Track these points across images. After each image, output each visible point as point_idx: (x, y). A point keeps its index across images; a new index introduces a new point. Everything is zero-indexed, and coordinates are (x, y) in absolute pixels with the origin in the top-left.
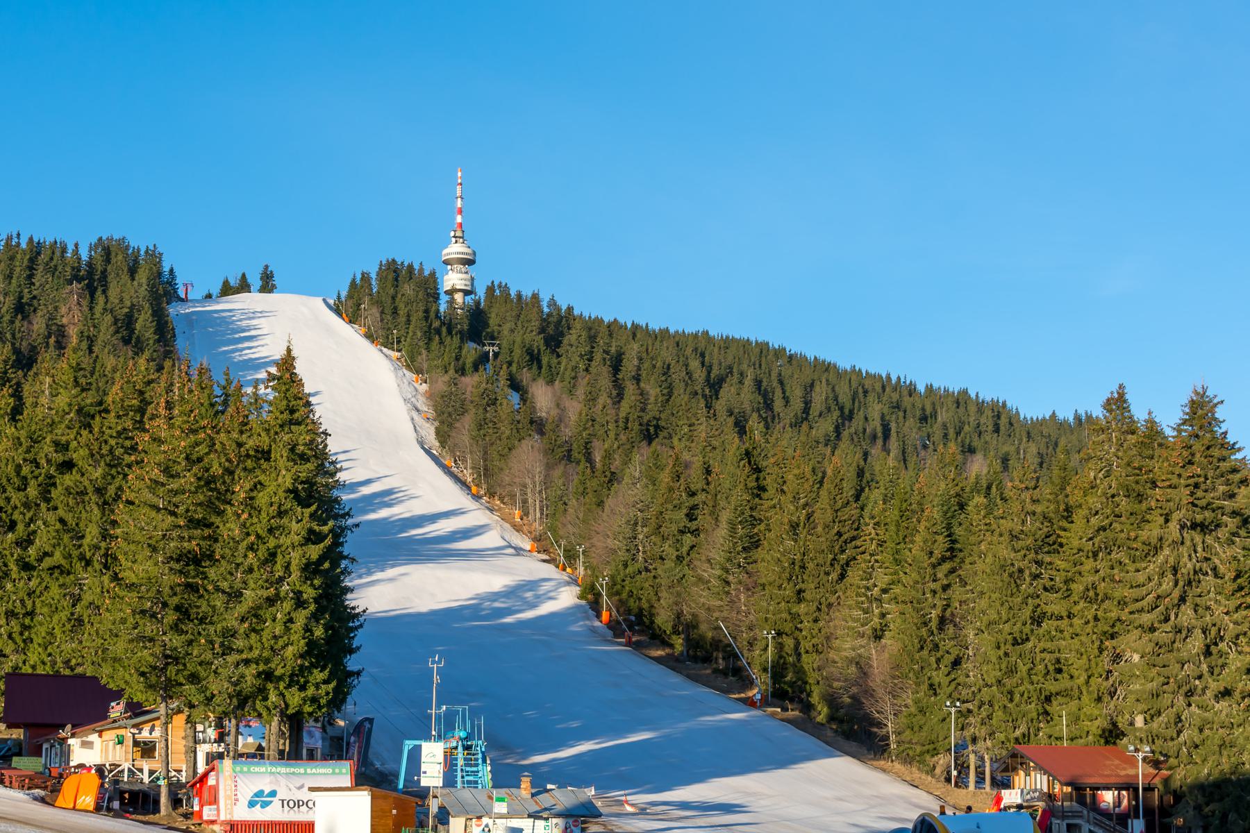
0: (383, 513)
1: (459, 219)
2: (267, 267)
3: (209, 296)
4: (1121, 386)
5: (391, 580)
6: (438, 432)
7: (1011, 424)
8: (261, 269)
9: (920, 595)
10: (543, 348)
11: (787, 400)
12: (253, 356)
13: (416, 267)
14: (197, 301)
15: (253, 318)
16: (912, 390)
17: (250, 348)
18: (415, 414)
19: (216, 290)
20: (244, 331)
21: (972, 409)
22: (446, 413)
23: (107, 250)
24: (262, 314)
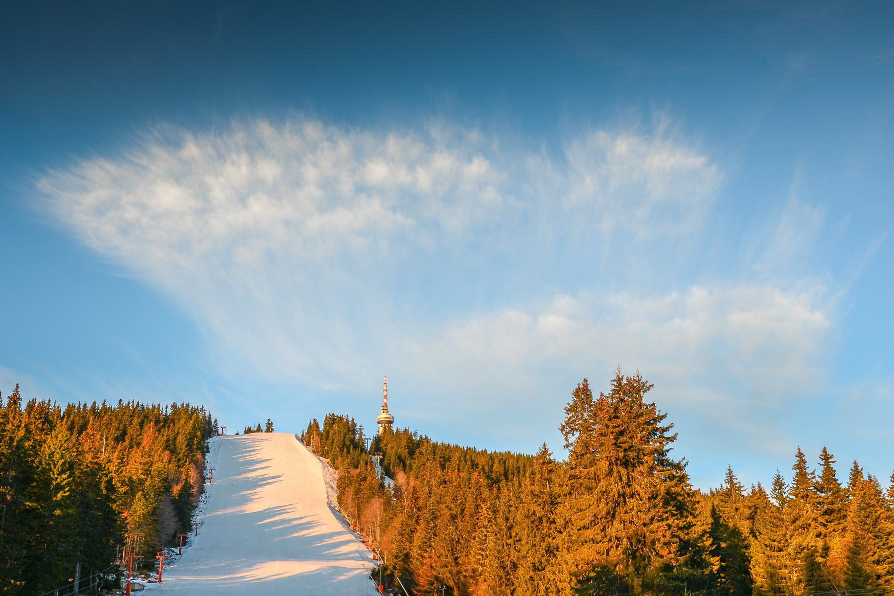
0: (304, 532)
3: (237, 434)
4: (585, 380)
9: (500, 548)
18: (329, 490)
23: (176, 410)
24: (263, 440)
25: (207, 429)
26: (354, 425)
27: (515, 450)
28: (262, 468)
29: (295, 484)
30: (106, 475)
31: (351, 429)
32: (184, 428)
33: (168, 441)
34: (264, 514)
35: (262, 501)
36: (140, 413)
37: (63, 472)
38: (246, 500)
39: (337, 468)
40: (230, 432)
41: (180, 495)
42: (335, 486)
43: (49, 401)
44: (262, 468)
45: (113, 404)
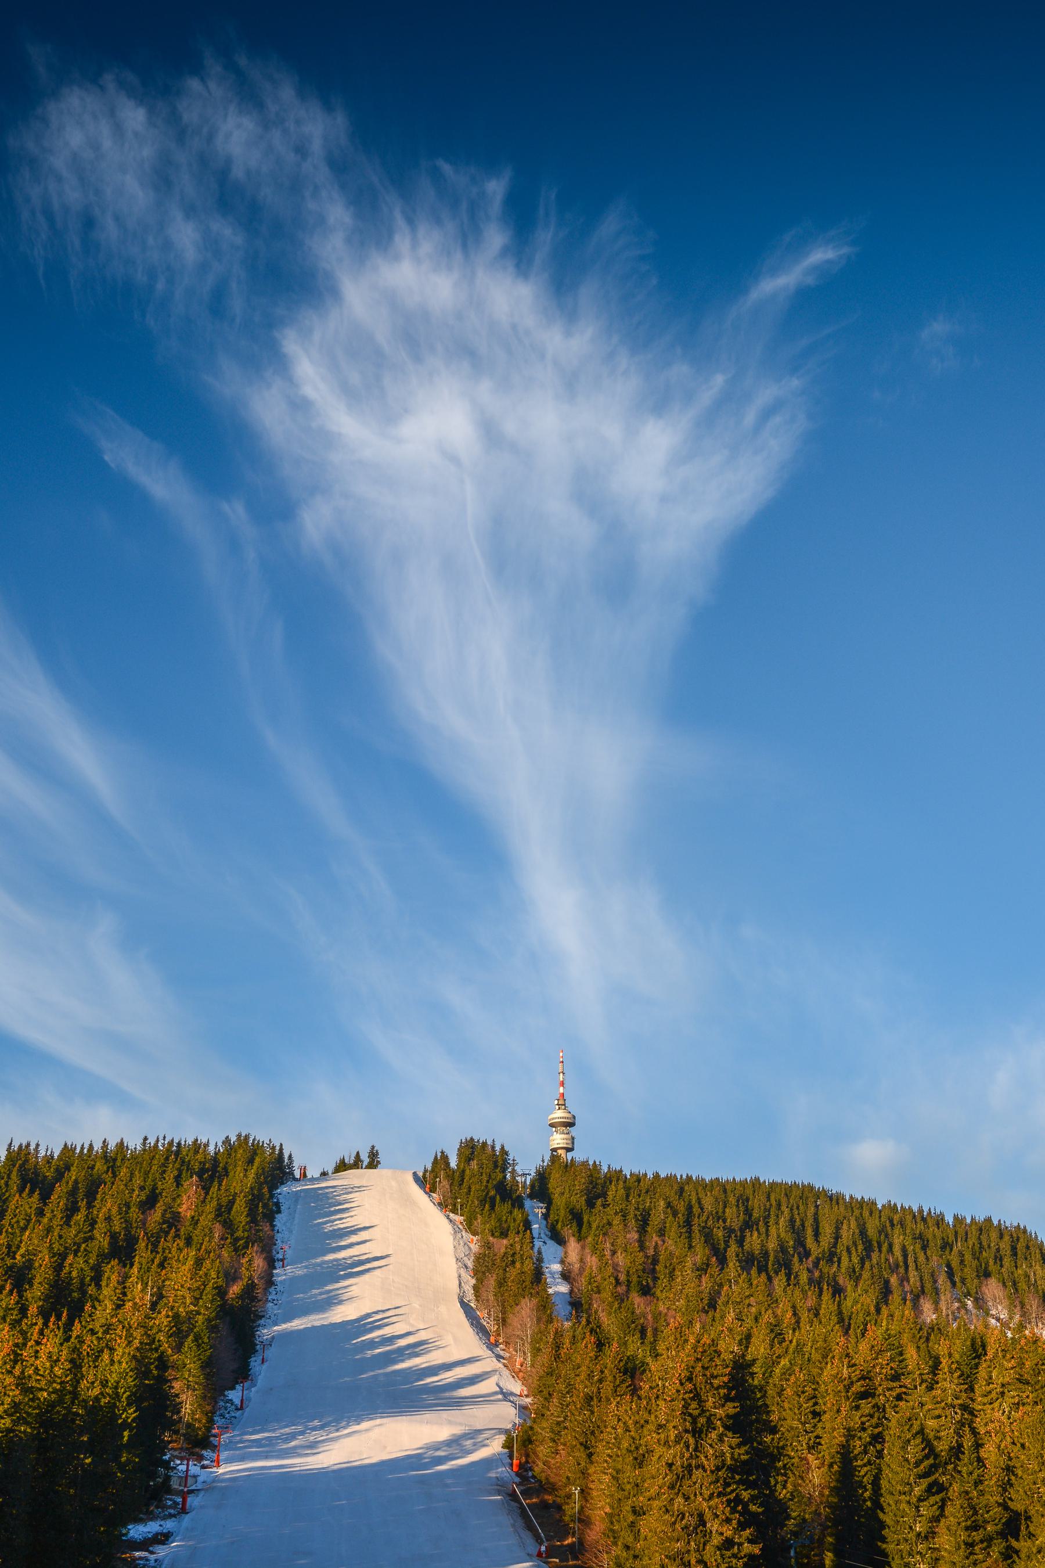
1: (561, 1090)
2: (373, 1147)
3: (324, 1174)
5: (367, 1430)
6: (476, 1288)
7: (1028, 1247)
8: (368, 1150)
10: (584, 1208)
11: (817, 1234)
12: (342, 1226)
13: (489, 1142)
14: (317, 1179)
15: (351, 1193)
16: (939, 1221)
17: (340, 1219)
18: (463, 1271)
19: (330, 1169)
20: (340, 1204)
21: (994, 1235)
22: (483, 1267)
24: (359, 1189)
25: (278, 1170)
26: (504, 1152)
27: (768, 1176)
28: (358, 1243)
29: (404, 1264)
30: (156, 1350)
31: (500, 1161)
32: (241, 1181)
34: (361, 1325)
35: (359, 1299)
36: (178, 1153)
37: (129, 1405)
38: (332, 1301)
39: (474, 1234)
40: (313, 1172)
41: (240, 1297)
42: (470, 1264)
43: (38, 1145)
44: (358, 1243)
45: (134, 1143)
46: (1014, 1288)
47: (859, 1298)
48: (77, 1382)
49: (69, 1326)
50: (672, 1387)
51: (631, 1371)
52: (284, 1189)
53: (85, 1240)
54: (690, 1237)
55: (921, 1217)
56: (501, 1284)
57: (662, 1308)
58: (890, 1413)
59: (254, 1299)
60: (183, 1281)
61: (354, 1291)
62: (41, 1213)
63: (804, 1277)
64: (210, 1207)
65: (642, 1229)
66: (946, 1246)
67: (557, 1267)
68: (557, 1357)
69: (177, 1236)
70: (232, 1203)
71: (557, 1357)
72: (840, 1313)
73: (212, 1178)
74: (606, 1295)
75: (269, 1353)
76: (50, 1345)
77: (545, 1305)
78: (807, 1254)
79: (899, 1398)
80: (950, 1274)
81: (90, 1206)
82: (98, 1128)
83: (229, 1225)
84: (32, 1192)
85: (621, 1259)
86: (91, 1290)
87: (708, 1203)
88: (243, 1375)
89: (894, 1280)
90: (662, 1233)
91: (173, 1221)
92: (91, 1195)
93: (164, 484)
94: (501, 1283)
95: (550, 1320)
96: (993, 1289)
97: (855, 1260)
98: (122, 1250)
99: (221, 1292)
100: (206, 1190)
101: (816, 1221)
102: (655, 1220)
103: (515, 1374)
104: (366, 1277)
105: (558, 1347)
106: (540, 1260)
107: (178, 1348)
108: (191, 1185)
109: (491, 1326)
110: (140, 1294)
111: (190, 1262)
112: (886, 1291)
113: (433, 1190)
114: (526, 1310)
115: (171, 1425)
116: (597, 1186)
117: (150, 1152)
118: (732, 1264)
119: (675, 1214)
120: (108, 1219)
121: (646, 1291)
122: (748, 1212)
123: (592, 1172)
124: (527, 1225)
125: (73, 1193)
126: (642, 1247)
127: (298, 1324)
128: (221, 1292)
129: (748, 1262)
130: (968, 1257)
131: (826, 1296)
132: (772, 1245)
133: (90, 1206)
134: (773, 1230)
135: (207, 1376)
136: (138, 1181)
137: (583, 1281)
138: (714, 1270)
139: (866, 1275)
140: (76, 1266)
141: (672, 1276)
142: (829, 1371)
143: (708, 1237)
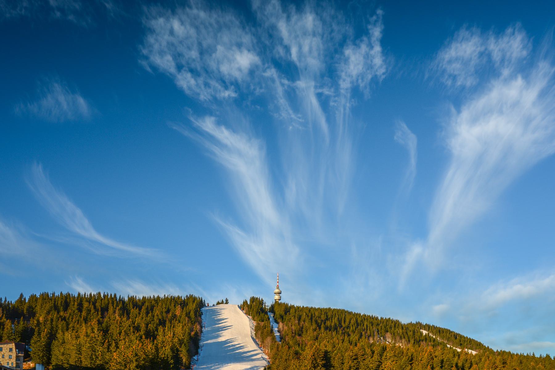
0: (241, 350)
11: (345, 322)
16: (377, 318)
19: (215, 304)
21: (390, 322)
24: (224, 309)
25: (201, 304)
29: (237, 327)
31: (261, 302)
32: (192, 306)
33: (186, 313)
34: (226, 342)
35: (225, 336)
36: (174, 299)
38: (218, 336)
40: (211, 305)
41: (194, 335)
45: (162, 296)
46: (394, 335)
47: (354, 337)
48: (158, 354)
49: (153, 341)
50: (309, 357)
51: (297, 354)
52: (203, 309)
53: (152, 320)
54: (312, 322)
55: (372, 318)
56: (262, 333)
57: (304, 339)
58: (361, 363)
59: (198, 336)
60: (180, 330)
61: (224, 334)
62: (139, 314)
63: (341, 332)
64: (184, 313)
65: (299, 319)
66: (378, 325)
67: (276, 329)
68: (278, 350)
69: (176, 320)
70: (190, 312)
71: (278, 350)
72: (349, 340)
73: (184, 306)
74: (290, 336)
75: (203, 348)
76: (150, 346)
77: (274, 338)
78: (342, 326)
79: (364, 360)
80: (378, 331)
81: (152, 312)
82: (141, 291)
83: (189, 317)
84: (136, 309)
85: (293, 327)
86: (156, 333)
87: (317, 314)
88: (197, 353)
89: (363, 333)
90: (304, 321)
91: (175, 316)
92: (152, 309)
93: (186, 133)
94: (262, 333)
95: (275, 342)
96: (388, 335)
97: (354, 328)
98: (162, 323)
99: (190, 334)
100: (183, 309)
101: (345, 318)
102: (303, 318)
103: (266, 354)
104: (226, 331)
105: (278, 348)
106: (272, 327)
107: (180, 347)
108: (178, 308)
109: (260, 343)
110: (170, 334)
111: (181, 327)
112: (361, 336)
113: (243, 310)
114: (269, 340)
115: (182, 364)
116: (287, 309)
117: (166, 299)
118: (322, 329)
119: (308, 316)
120: (158, 315)
121: (300, 335)
122: (327, 316)
123: (286, 305)
124: (269, 319)
125: (147, 309)
126: (299, 325)
127: (209, 341)
128: (190, 334)
129: (326, 328)
130: (383, 327)
131: (346, 337)
132: (333, 324)
133: (152, 312)
134: (333, 321)
135: (189, 353)
136: (164, 306)
137: (283, 333)
138: (318, 330)
139: (356, 332)
140: (151, 327)
141: (307, 331)
142: (347, 354)
143: (316, 322)
